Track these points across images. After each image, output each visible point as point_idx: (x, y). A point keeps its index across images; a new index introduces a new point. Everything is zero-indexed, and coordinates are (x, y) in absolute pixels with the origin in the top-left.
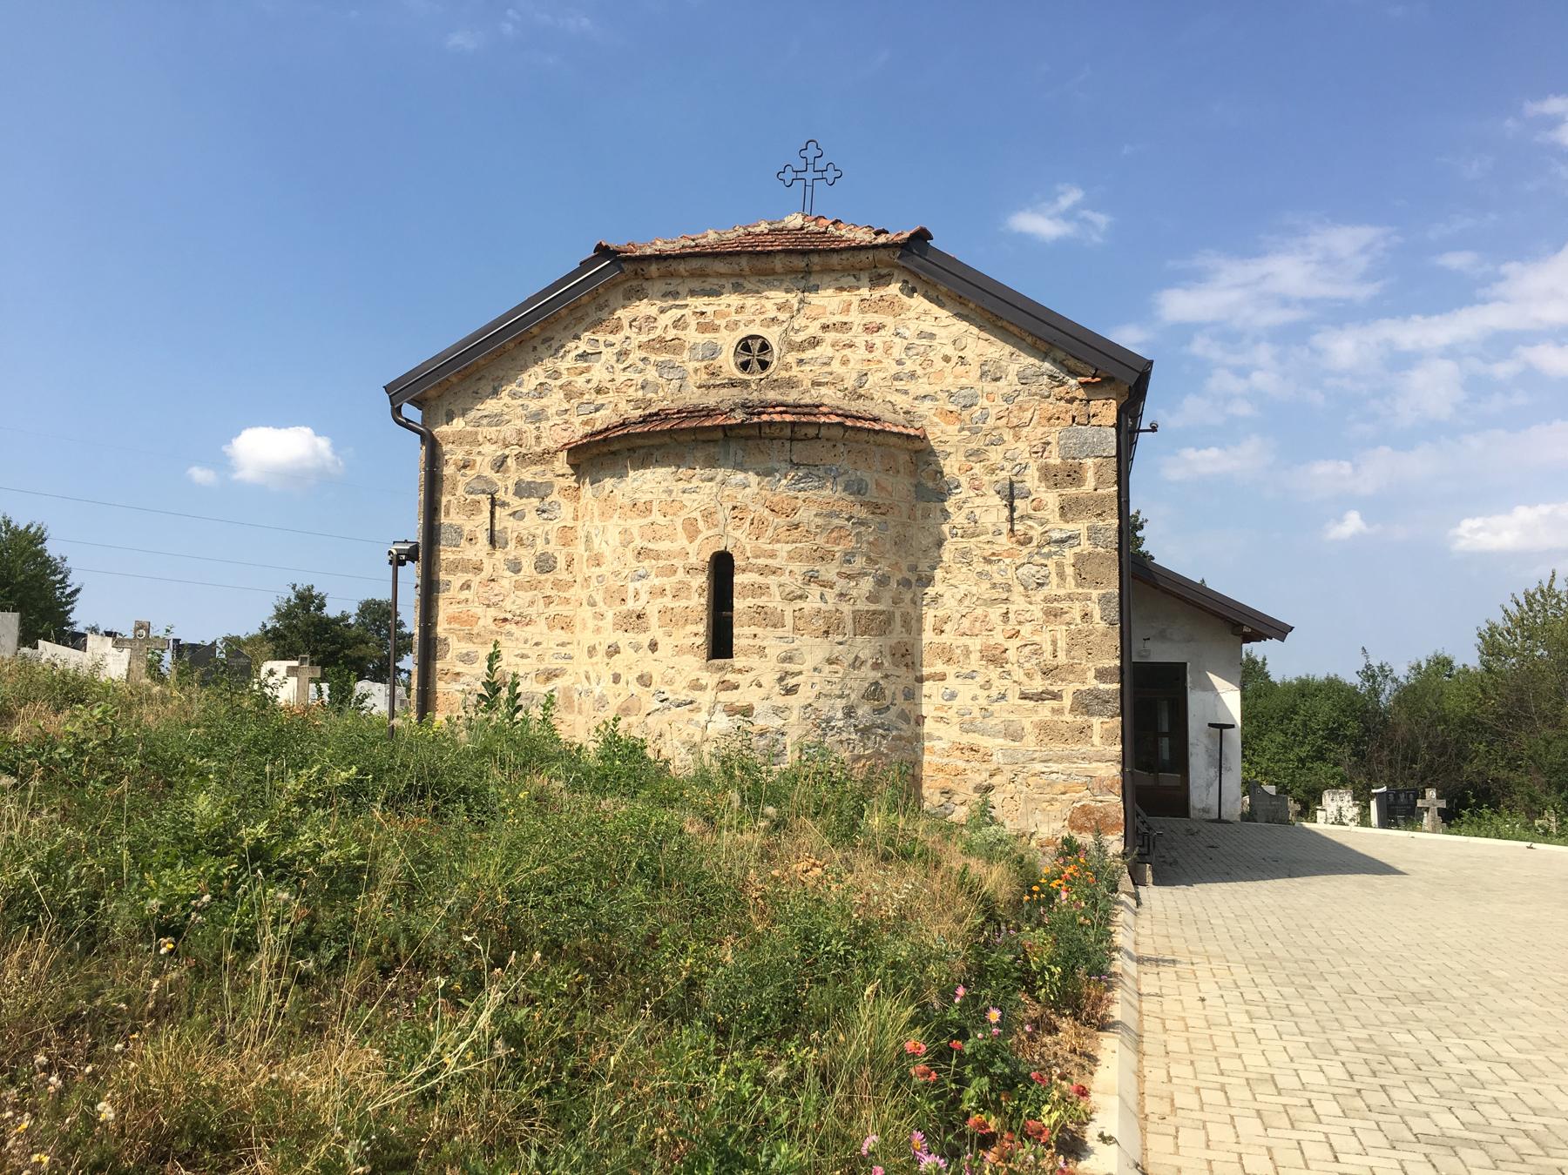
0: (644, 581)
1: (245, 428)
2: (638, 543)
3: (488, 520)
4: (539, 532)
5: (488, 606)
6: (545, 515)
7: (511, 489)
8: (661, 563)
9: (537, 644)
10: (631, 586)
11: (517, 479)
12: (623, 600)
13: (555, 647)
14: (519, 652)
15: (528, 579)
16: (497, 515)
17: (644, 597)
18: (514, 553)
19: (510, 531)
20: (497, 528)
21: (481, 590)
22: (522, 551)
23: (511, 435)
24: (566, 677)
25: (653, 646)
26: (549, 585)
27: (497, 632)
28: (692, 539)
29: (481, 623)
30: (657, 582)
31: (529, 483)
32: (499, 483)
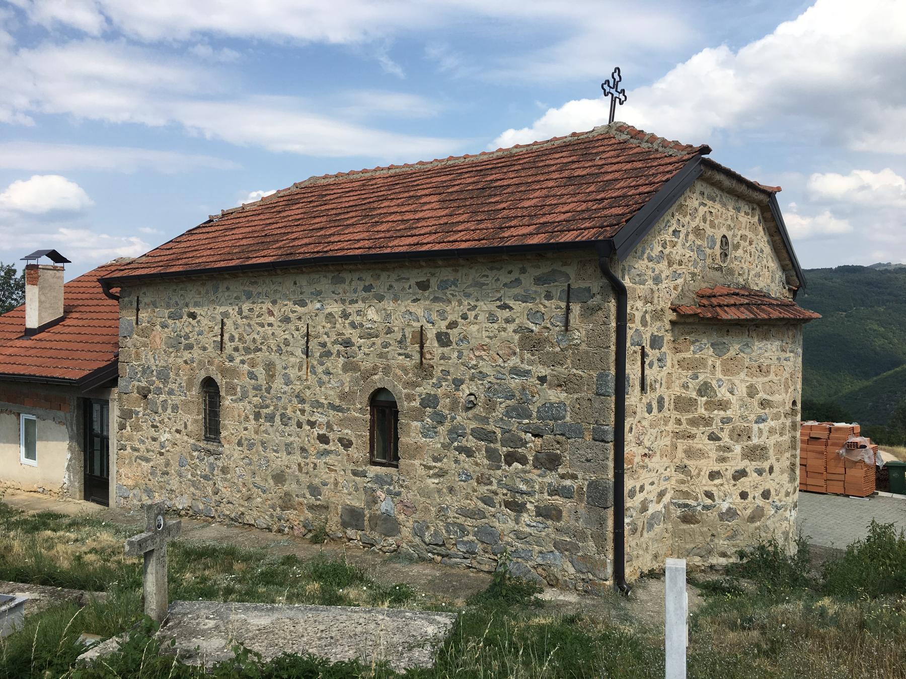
0: (766, 424)
2: (762, 395)
8: (775, 411)
10: (755, 427)
17: (765, 434)
25: (771, 470)
28: (787, 392)
30: (773, 423)
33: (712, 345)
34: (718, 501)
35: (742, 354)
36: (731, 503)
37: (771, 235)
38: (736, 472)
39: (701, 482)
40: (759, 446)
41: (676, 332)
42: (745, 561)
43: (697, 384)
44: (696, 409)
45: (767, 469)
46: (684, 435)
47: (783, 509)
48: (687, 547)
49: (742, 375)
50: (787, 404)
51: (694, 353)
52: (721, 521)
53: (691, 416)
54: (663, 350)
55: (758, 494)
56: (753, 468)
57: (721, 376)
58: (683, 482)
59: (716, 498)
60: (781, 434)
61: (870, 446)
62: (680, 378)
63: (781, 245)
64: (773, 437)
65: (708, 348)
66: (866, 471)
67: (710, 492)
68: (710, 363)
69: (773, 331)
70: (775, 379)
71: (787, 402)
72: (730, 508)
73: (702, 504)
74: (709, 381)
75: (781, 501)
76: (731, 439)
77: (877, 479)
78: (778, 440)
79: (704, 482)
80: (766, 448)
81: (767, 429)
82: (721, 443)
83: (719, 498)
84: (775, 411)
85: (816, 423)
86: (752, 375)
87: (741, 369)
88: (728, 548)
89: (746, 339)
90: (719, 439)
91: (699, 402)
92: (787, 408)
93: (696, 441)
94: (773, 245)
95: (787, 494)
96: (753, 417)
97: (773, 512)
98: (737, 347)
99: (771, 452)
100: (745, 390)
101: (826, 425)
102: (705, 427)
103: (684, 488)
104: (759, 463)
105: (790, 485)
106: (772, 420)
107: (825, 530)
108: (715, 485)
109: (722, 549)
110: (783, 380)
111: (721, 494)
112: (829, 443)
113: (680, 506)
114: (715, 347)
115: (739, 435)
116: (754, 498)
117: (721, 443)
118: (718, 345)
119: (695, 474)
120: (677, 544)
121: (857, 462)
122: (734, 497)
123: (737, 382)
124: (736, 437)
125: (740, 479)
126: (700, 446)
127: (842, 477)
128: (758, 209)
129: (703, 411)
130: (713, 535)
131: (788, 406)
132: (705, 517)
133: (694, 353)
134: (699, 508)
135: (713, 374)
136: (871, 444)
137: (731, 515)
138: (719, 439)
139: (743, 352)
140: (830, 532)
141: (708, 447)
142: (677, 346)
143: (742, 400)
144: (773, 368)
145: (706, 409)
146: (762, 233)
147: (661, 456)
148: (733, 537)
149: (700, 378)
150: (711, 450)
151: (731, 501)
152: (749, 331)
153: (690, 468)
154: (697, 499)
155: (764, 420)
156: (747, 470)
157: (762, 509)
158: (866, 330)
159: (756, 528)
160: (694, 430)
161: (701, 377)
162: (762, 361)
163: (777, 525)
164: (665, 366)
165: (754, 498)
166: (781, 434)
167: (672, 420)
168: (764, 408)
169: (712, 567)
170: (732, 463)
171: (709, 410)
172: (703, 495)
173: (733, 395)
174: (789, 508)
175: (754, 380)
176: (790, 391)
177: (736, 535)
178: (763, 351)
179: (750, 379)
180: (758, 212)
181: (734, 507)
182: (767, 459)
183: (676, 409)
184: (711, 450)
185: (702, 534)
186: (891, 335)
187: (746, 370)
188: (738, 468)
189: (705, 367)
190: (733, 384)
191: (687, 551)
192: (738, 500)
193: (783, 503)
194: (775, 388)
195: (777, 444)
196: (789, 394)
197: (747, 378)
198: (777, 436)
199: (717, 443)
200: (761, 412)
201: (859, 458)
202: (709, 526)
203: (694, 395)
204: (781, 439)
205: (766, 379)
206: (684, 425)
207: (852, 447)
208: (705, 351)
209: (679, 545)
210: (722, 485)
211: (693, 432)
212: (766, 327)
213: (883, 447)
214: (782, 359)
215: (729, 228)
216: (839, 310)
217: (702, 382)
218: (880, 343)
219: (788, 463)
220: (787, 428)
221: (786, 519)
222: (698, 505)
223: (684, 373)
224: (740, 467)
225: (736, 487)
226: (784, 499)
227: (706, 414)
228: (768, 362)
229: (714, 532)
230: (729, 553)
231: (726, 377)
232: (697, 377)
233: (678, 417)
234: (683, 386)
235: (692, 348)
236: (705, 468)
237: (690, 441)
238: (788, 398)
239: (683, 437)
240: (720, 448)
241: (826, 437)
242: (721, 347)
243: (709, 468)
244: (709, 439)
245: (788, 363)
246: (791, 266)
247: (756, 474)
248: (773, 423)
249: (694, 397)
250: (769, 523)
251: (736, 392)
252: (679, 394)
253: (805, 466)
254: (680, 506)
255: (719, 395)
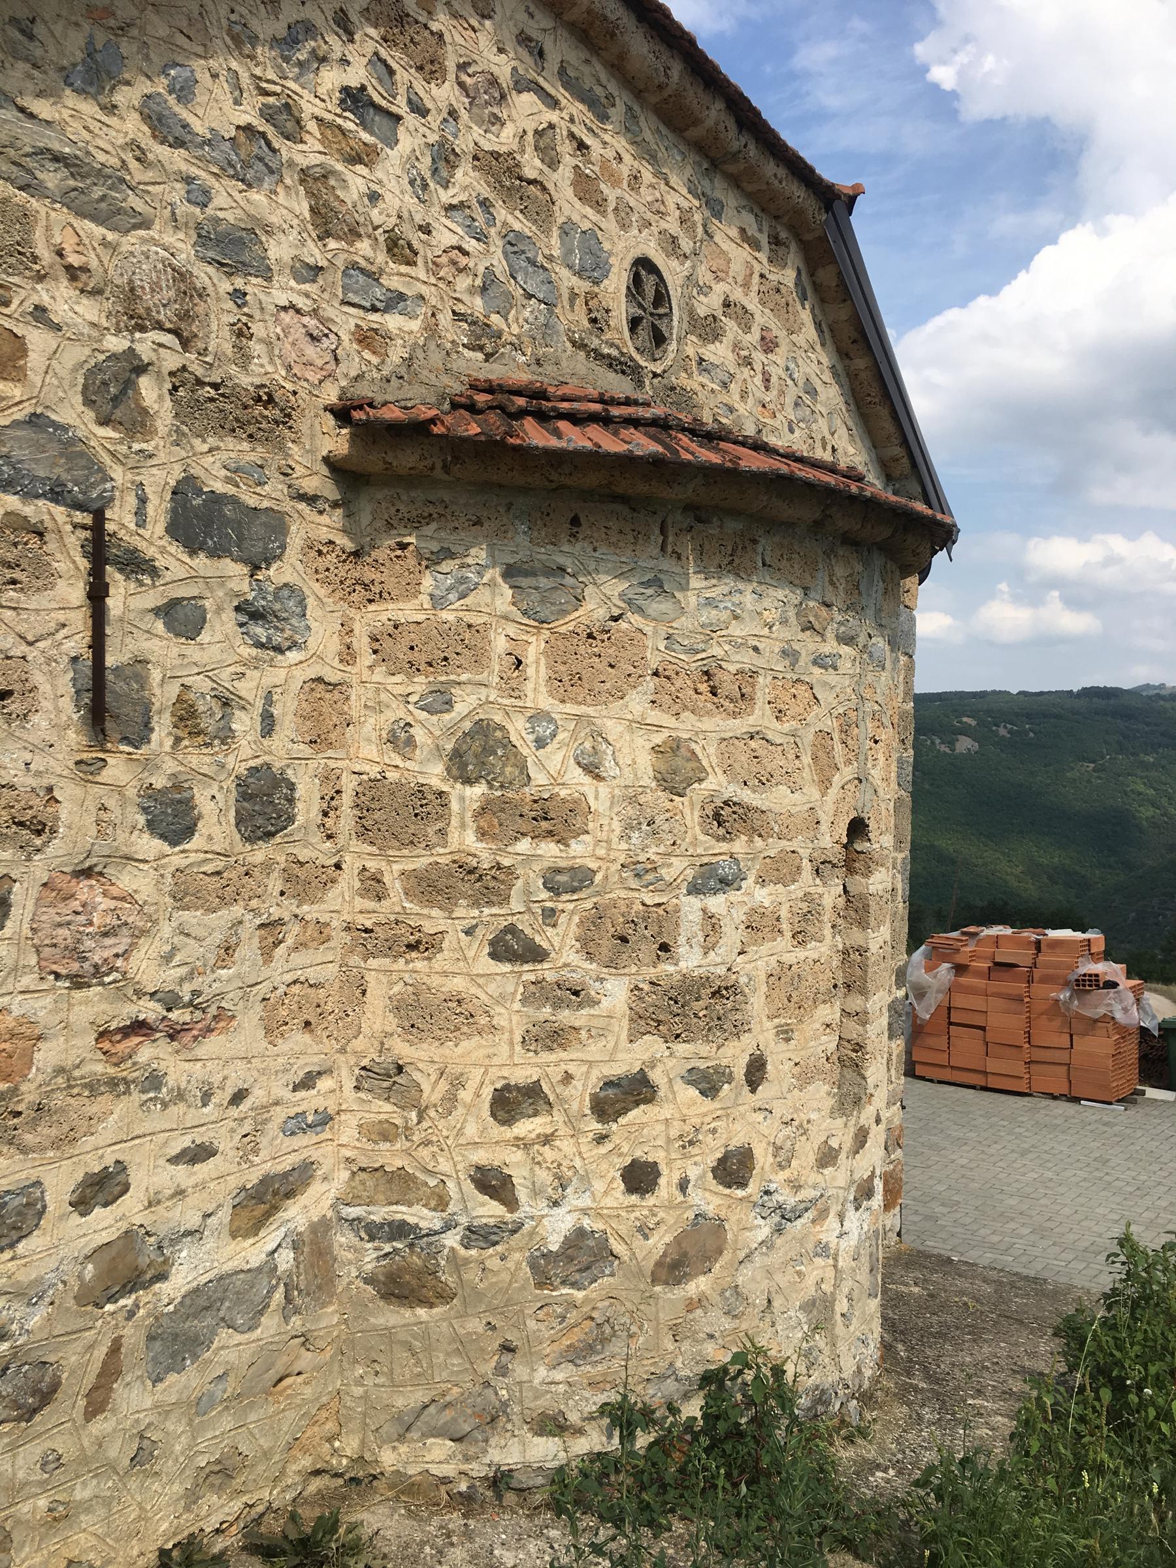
0: (734, 896)
1: (950, 307)
2: (717, 784)
3: (80, 620)
4: (245, 688)
5: (78, 982)
6: (260, 631)
7: (158, 509)
8: (774, 847)
9: (238, 1097)
10: (691, 907)
11: (177, 473)
12: (664, 947)
13: (286, 1094)
14: (185, 1142)
15: (219, 864)
16: (114, 604)
17: (732, 936)
18: (170, 766)
19: (156, 675)
20: (110, 661)
21: (49, 915)
22: (198, 759)
23: (155, 288)
24: (316, 1188)
25: (756, 1072)
26: (275, 884)
27: (113, 1083)
28: (825, 784)
29: (47, 1056)
30: (763, 896)
31: (216, 499)
32: (118, 474)
33: (510, 573)
34: (528, 1206)
35: (636, 619)
36: (585, 1211)
37: (843, 354)
38: (609, 1084)
39: (460, 1133)
40: (706, 981)
41: (365, 518)
42: (643, 1440)
43: (450, 731)
44: (442, 832)
45: (740, 1071)
46: (395, 939)
47: (809, 1215)
48: (400, 1402)
49: (637, 703)
50: (824, 827)
51: (438, 602)
52: (540, 1285)
53: (421, 863)
54: (279, 574)
55: (700, 1165)
56: (676, 1067)
57: (546, 702)
58: (385, 1133)
59: (522, 1194)
60: (800, 937)
61: (1125, 983)
62: (378, 708)
63: (874, 391)
64: (765, 948)
65: (491, 584)
66: (1117, 1043)
67: (498, 1170)
68: (500, 644)
69: (766, 546)
70: (776, 730)
71: (824, 819)
72: (580, 1233)
73: (464, 1220)
74: (498, 718)
75: (797, 1187)
76: (590, 956)
77: (1143, 1058)
78: (789, 958)
79: (471, 1130)
80: (733, 988)
81: (739, 915)
82: (547, 972)
83: (535, 1192)
84: (774, 847)
85: (1009, 931)
86: (678, 707)
87: (632, 679)
88: (568, 1396)
89: (649, 559)
90: (536, 954)
91: (455, 806)
92: (826, 841)
93: (440, 961)
94: (853, 390)
95: (828, 1157)
96: (678, 868)
97: (764, 1231)
98: (615, 587)
99: (757, 1004)
100: (645, 763)
101: (1030, 935)
102: (476, 904)
103: (391, 1157)
104: (704, 1049)
105: (840, 1122)
106: (762, 881)
107: (1013, 1202)
108: (521, 1143)
109: (544, 1404)
110: (808, 736)
111: (544, 1176)
112: (1036, 976)
113: (373, 1232)
114: (524, 582)
115: (624, 940)
116: (683, 1186)
117: (547, 972)
118: (533, 573)
119: (436, 1097)
120: (358, 1391)
121: (1096, 1021)
122: (599, 1186)
123: (613, 728)
124: (607, 945)
125: (625, 1111)
126: (458, 984)
127: (1063, 1056)
128: (793, 247)
129: (470, 839)
130: (507, 1348)
131: (831, 838)
132: (472, 1275)
133: (438, 602)
134: (451, 1240)
135: (515, 692)
136: (1128, 978)
137: (585, 1259)
138: (536, 954)
139: (640, 610)
140: (1024, 1207)
141: (492, 988)
142: (369, 575)
143: (633, 800)
144: (763, 686)
145: (482, 834)
146: (810, 332)
147: (273, 1029)
148: (590, 1349)
149: (460, 708)
150: (501, 999)
151: (586, 1201)
152: (663, 531)
153: (417, 1076)
154: (441, 1203)
155: (726, 883)
156: (656, 1076)
157: (719, 1226)
158: (1126, 793)
159: (692, 1305)
160: (433, 920)
161: (465, 703)
162: (717, 651)
163: (781, 1279)
164: (294, 645)
165: (683, 1186)
166: (800, 937)
167: (348, 880)
168: (728, 837)
169: (500, 1481)
170: (594, 1050)
171: (494, 837)
172: (469, 1187)
173: (598, 777)
174: (834, 1209)
175: (685, 726)
176: (837, 780)
177: (605, 1341)
178: (725, 615)
179: (668, 720)
180: (794, 258)
181: (599, 1226)
182: (739, 1030)
183: (363, 832)
184: (501, 999)
185: (462, 1346)
186: (1164, 801)
187: (650, 683)
188: (617, 1070)
189: (479, 660)
190: (598, 735)
191: (398, 1418)
192: (618, 1196)
193: (807, 1194)
194: (775, 762)
195: (779, 975)
196: (834, 792)
197: (654, 716)
198: (784, 943)
199: (529, 972)
200: (710, 847)
201: (1102, 1011)
202: (492, 1310)
203: (434, 775)
204: (801, 953)
205: (739, 726)
206: (397, 899)
207: (1093, 983)
208: (479, 598)
209: (365, 1397)
210: (547, 1140)
211: (429, 928)
212: (732, 525)
213: (1154, 986)
214: (804, 660)
215: (671, 244)
216: (1084, 759)
217: (467, 725)
218: (1149, 814)
219: (829, 1042)
220: (828, 916)
221: (823, 1250)
222: (448, 1226)
223: (397, 683)
224: (626, 1063)
225: (608, 1146)
226: (814, 1177)
227: (483, 853)
228: (746, 659)
229: (512, 1336)
230: (574, 1418)
231: (570, 708)
232: (449, 704)
233: (372, 865)
234: (392, 740)
235: (428, 582)
236: (476, 1074)
237: (419, 965)
238: (830, 807)
239: (390, 949)
240: (538, 993)
241: (1029, 963)
242: (543, 582)
243: (494, 1072)
244: (494, 955)
245: (831, 677)
246: (905, 461)
247: (693, 1092)
248: (763, 896)
249: (436, 783)
250: (743, 1277)
251: (608, 767)
252: (374, 771)
253: (983, 1029)
254: (373, 1232)
255: (539, 778)
